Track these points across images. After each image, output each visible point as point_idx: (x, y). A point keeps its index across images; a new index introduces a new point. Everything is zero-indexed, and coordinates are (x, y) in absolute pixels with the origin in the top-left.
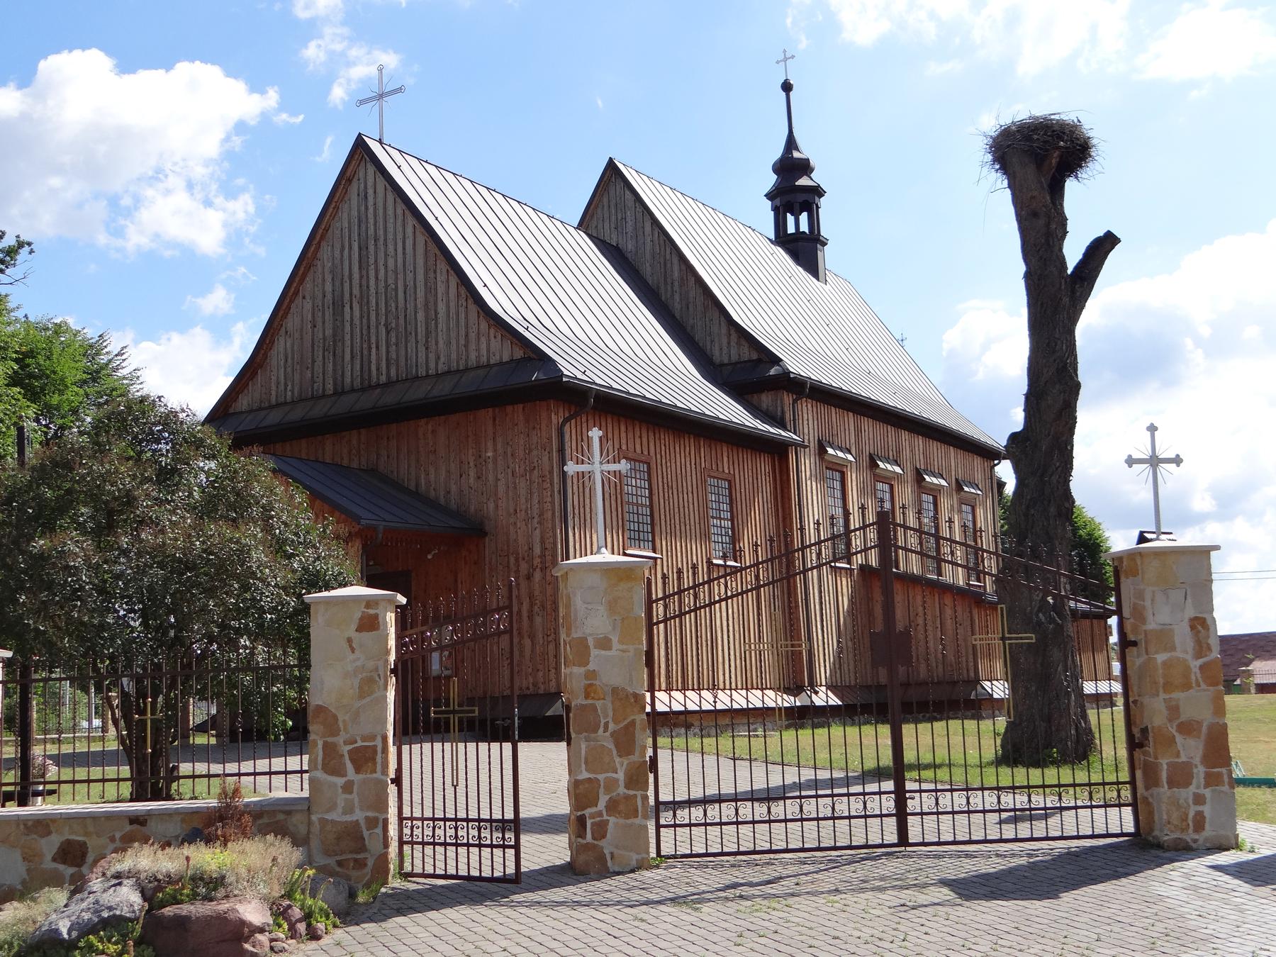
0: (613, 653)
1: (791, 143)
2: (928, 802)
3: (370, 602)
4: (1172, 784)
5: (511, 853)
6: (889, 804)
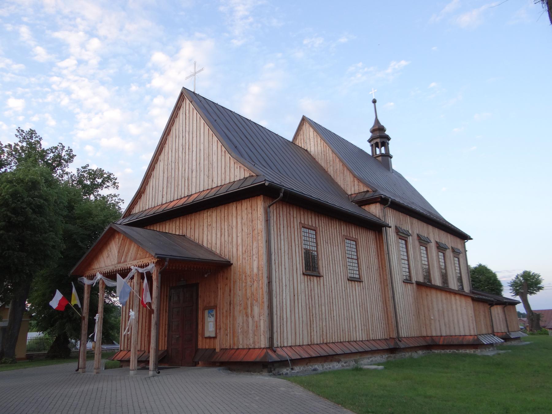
1: (377, 121)
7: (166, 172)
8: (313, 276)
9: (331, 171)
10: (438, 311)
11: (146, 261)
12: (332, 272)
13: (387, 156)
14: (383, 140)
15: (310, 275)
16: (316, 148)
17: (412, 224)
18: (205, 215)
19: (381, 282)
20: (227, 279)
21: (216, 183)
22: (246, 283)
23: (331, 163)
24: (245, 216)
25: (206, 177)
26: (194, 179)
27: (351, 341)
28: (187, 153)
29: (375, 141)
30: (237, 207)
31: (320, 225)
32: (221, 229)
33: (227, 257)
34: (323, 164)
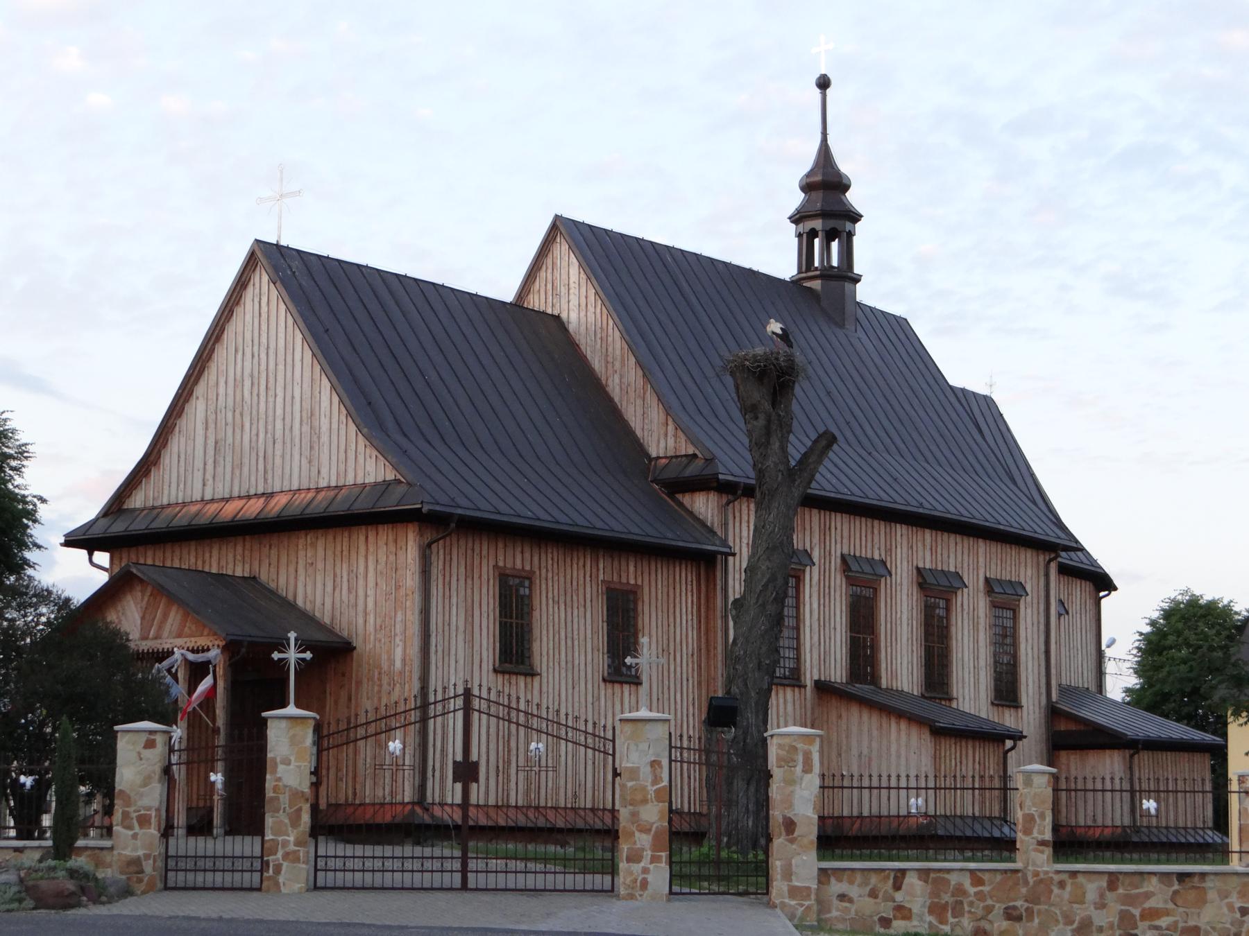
0: (291, 767)
1: (825, 154)
2: (481, 865)
3: (151, 732)
4: (629, 860)
5: (172, 852)
6: (457, 865)
7: (211, 426)
8: (517, 674)
9: (614, 387)
10: (860, 756)
11: (202, 642)
12: (563, 664)
13: (845, 276)
14: (832, 223)
15: (510, 673)
16: (583, 314)
17: (825, 531)
18: (302, 541)
19: (699, 683)
20: (343, 675)
21: (326, 481)
22: (380, 686)
23: (618, 365)
24: (382, 559)
25: (304, 462)
26: (278, 461)
27: (598, 809)
28: (263, 399)
29: (810, 224)
30: (367, 538)
31: (543, 564)
32: (335, 575)
33: (345, 634)
34: (597, 364)
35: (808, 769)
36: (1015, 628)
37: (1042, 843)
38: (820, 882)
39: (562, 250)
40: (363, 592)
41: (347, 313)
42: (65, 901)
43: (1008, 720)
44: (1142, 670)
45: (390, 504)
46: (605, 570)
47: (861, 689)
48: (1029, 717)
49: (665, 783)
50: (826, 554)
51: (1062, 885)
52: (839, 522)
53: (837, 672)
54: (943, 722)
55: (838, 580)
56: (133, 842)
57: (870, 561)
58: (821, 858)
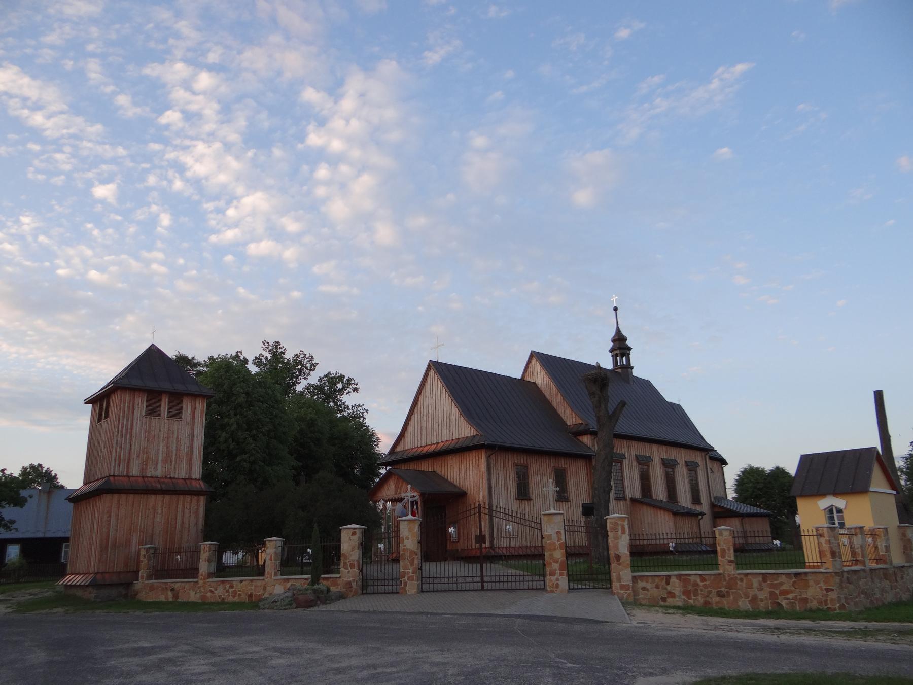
1: (618, 331)
3: (354, 529)
4: (550, 575)
9: (554, 404)
13: (628, 367)
17: (629, 447)
34: (548, 397)
35: (623, 532)
36: (697, 478)
37: (730, 561)
38: (633, 582)
39: (534, 361)
40: (468, 475)
41: (460, 383)
42: (309, 604)
43: (698, 509)
44: (737, 491)
45: (475, 443)
46: (553, 462)
47: (647, 500)
48: (705, 507)
49: (563, 541)
50: (630, 455)
51: (741, 580)
52: (634, 444)
53: (638, 494)
54: (676, 510)
55: (635, 463)
56: (348, 574)
57: (645, 456)
58: (632, 572)
